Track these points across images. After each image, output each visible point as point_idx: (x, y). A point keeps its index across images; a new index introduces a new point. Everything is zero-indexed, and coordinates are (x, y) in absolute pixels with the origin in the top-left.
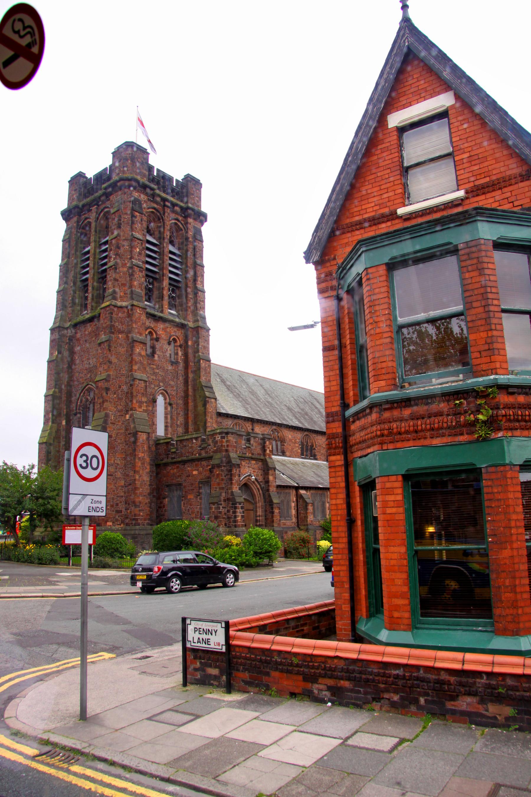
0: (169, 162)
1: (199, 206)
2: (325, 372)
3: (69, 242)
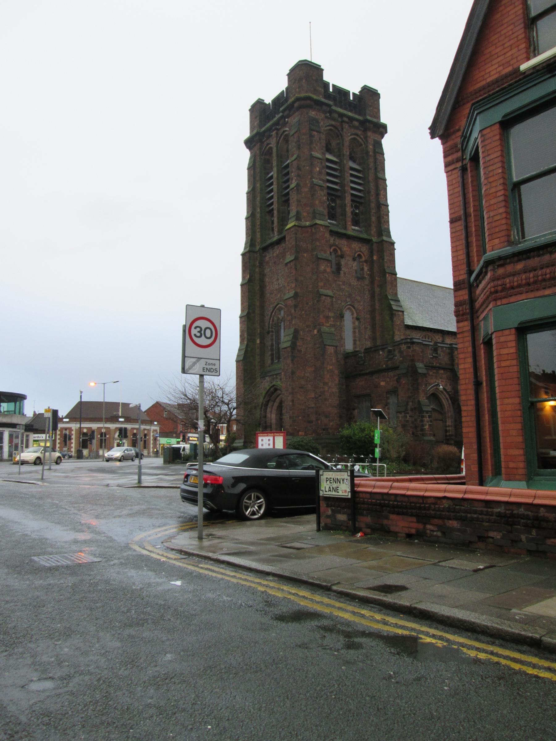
0: (344, 75)
1: (378, 117)
2: (452, 242)
3: (252, 168)
